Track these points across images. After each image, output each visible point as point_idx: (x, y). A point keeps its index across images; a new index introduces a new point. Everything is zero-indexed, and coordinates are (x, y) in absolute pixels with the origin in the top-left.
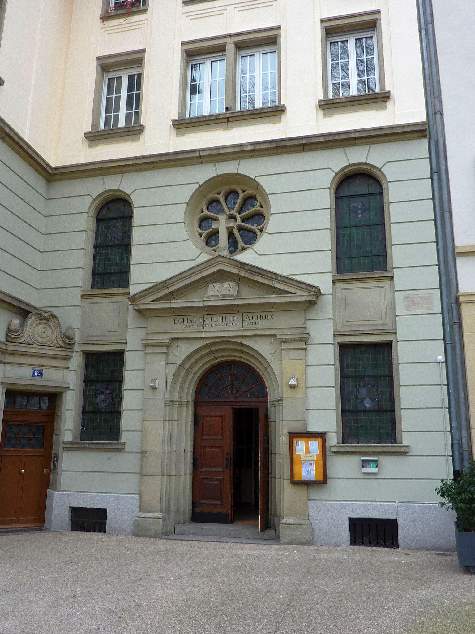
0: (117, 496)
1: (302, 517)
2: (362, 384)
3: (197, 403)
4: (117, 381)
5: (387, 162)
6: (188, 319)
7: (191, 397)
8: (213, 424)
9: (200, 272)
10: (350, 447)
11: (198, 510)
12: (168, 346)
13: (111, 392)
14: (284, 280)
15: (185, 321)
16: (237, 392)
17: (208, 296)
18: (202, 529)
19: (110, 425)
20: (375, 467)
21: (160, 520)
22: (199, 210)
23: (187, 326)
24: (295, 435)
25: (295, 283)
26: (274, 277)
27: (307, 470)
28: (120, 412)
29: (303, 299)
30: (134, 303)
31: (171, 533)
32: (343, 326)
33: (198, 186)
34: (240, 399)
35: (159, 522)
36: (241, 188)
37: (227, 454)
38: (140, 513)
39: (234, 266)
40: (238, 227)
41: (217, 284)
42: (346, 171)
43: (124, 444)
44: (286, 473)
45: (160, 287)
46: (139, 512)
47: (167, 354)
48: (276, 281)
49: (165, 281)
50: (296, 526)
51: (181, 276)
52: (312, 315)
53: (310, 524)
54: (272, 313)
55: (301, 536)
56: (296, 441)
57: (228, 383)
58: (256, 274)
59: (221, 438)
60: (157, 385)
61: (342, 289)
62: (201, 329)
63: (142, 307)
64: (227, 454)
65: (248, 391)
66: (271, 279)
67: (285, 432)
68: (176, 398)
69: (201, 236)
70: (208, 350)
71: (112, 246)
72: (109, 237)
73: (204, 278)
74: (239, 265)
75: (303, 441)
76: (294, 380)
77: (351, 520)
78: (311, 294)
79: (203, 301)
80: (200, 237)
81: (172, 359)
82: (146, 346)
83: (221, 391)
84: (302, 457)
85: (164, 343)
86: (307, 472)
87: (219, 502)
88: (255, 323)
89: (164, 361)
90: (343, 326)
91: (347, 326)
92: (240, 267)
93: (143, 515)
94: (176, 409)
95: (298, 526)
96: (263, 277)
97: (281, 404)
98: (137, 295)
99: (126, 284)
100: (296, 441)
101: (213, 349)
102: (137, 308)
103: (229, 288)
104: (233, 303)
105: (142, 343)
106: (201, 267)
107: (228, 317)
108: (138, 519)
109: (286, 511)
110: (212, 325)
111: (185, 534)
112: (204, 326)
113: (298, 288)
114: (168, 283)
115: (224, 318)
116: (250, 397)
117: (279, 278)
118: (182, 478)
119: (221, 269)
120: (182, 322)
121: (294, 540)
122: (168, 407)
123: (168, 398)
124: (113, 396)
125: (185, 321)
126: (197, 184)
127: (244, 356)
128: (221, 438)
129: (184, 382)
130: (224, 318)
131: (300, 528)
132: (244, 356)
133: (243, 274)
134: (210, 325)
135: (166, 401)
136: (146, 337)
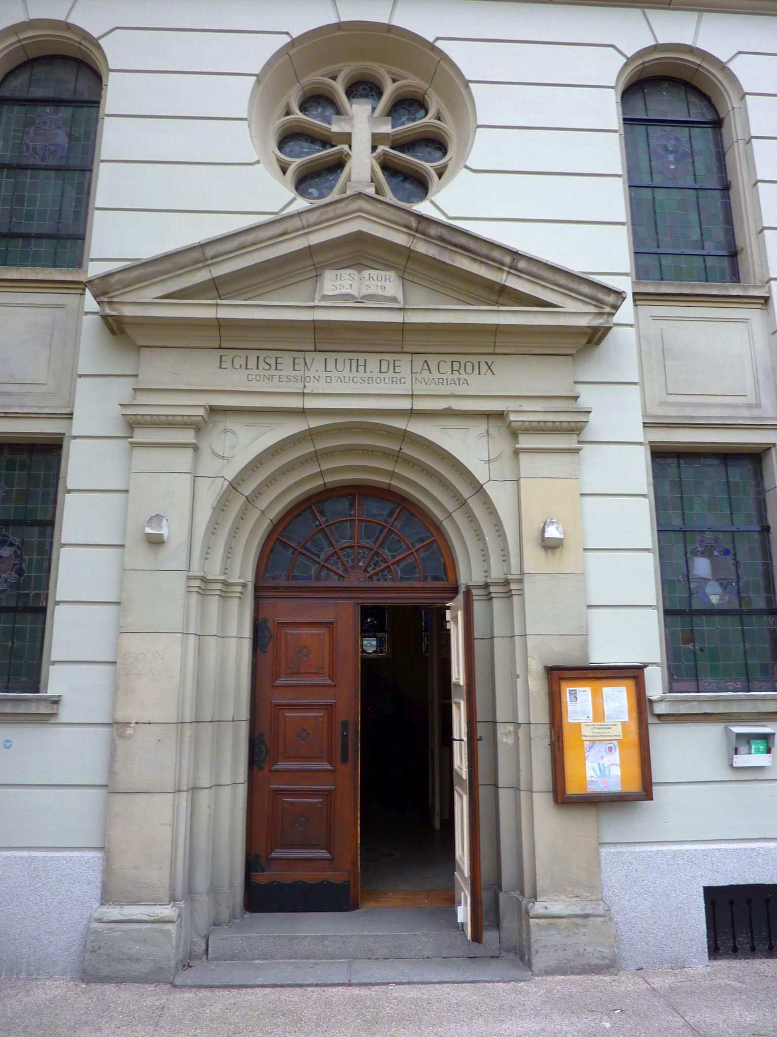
0: (30, 857)
1: (585, 894)
2: (698, 547)
3: (260, 590)
4: (35, 523)
5: (740, 53)
6: (261, 360)
7: (249, 576)
8: (305, 647)
9: (303, 232)
10: (699, 701)
11: (262, 878)
12: (198, 427)
13: (15, 552)
14: (534, 269)
15: (252, 363)
16: (368, 565)
17: (325, 297)
18: (291, 939)
19: (10, 644)
20: (762, 752)
21: (170, 927)
22: (281, 108)
23: (258, 378)
24: (568, 674)
25: (562, 280)
26: (507, 260)
27: (599, 764)
28: (44, 610)
29: (584, 322)
30: (106, 299)
31: (198, 957)
32: (662, 404)
33: (286, 39)
34: (375, 583)
35: (167, 933)
36: (389, 73)
37: (345, 725)
38: (104, 909)
39: (397, 227)
40: (382, 158)
41: (348, 271)
42: (647, 59)
43: (56, 701)
44: (541, 775)
45: (186, 259)
46: (102, 904)
47: (195, 448)
49: (202, 246)
50: (574, 920)
51: (249, 238)
52: (590, 370)
53: (607, 916)
54: (490, 359)
55: (590, 949)
56: (567, 689)
57: (345, 543)
58: (460, 251)
59: (329, 682)
60: (164, 531)
61: (656, 318)
62: (297, 387)
63: (128, 311)
64: (345, 725)
65: (397, 563)
66: (499, 266)
67: (536, 666)
68: (215, 573)
69: (284, 171)
70: (307, 449)
71: (35, 168)
72: (28, 145)
73: (310, 251)
74: (414, 224)
75: (588, 690)
76: (557, 528)
77: (709, 892)
78: (602, 310)
80: (282, 174)
81: (209, 466)
82: (133, 424)
83: (325, 561)
84: (586, 731)
85: (189, 416)
86: (600, 770)
87: (324, 854)
88: (445, 381)
89: (187, 467)
90: (662, 404)
91: (667, 404)
92: (417, 231)
93: (114, 912)
94: (214, 603)
95: (580, 921)
96: (475, 260)
97: (520, 592)
98: (117, 277)
99: (78, 263)
100: (567, 689)
101: (321, 445)
102: (114, 313)
103: (383, 283)
104: (396, 318)
105: (123, 415)
106: (307, 220)
107: (373, 362)
108: (95, 925)
109: (543, 882)
110: (329, 379)
111: (239, 959)
112: (305, 379)
113: (570, 293)
114: (210, 252)
115: (361, 362)
116: (402, 579)
117: (522, 265)
118: (226, 793)
119: (360, 231)
120: (243, 367)
121: (569, 961)
122: (194, 598)
123: (196, 570)
124: (21, 564)
125: (252, 363)
126: (285, 36)
127: (401, 470)
128: (329, 682)
129: (235, 532)
130: (361, 362)
131: (585, 926)
132: (401, 470)
133: (422, 247)
134: (322, 380)
135: (189, 578)
136: (134, 398)
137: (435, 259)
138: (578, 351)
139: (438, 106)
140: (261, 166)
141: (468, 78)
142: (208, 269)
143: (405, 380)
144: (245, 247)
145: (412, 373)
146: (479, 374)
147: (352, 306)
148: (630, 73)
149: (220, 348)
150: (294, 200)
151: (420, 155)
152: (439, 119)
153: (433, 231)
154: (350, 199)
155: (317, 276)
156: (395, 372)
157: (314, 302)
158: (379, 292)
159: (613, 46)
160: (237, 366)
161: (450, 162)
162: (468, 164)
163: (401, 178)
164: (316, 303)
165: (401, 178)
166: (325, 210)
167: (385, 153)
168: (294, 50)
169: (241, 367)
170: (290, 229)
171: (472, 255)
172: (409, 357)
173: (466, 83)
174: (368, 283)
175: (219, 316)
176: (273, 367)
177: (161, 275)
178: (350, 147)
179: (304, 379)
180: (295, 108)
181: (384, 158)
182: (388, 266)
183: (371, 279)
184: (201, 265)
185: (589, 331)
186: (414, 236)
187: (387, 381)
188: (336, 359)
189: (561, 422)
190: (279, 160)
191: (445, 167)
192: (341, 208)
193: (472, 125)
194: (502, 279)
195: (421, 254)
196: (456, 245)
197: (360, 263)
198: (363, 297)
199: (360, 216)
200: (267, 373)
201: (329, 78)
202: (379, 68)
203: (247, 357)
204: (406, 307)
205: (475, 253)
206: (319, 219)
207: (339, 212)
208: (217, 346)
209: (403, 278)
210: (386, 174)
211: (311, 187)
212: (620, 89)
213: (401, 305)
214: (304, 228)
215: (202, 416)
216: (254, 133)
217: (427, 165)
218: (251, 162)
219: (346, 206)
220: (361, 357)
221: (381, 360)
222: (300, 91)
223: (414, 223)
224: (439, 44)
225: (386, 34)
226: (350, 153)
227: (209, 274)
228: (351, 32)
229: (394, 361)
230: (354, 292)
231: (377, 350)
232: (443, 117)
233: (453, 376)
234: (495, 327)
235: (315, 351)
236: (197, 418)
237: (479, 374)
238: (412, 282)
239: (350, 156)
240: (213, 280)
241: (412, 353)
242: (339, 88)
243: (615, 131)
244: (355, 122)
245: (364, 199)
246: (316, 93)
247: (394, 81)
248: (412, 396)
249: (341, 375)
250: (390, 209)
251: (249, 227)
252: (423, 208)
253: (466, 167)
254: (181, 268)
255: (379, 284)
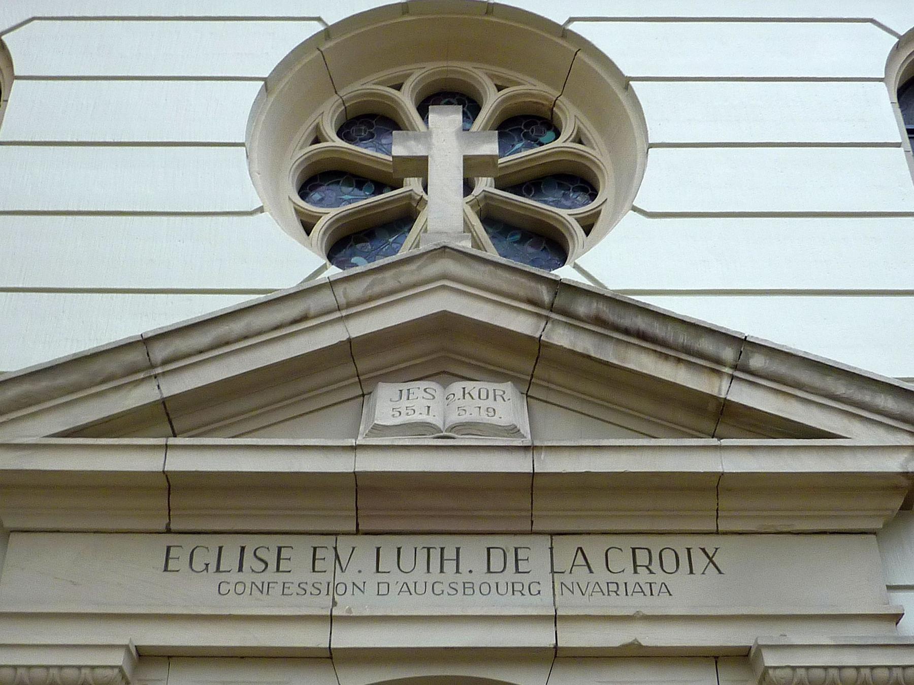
6: (248, 554)
9: (337, 315)
15: (230, 560)
22: (306, 130)
25: (840, 388)
26: (728, 354)
33: (318, 27)
36: (491, 77)
48: (738, 374)
49: (146, 342)
51: (237, 327)
54: (710, 543)
62: (319, 606)
66: (713, 365)
69: (308, 229)
74: (546, 297)
79: (351, 447)
88: (622, 588)
92: (551, 308)
96: (667, 357)
103: (490, 403)
104: (520, 464)
106: (345, 294)
112: (335, 588)
114: (160, 352)
115: (450, 554)
117: (757, 362)
120: (213, 567)
125: (230, 560)
130: (450, 554)
134: (371, 588)
137: (589, 357)
138: (886, 525)
139: (578, 122)
140: (266, 215)
141: (627, 73)
142: (154, 383)
143: (538, 588)
144: (227, 343)
145: (553, 572)
146: (691, 572)
147: (430, 444)
148: (897, 76)
149: (169, 531)
150: (323, 268)
151: (551, 199)
152: (580, 142)
153: (583, 308)
154: (425, 257)
155: (363, 395)
156: (517, 571)
157: (356, 439)
158: (484, 418)
159: (872, 21)
160: (198, 565)
161: (603, 207)
162: (636, 203)
163: (518, 237)
164: (361, 441)
165: (518, 237)
166: (379, 276)
167: (487, 196)
168: (330, 44)
169: (207, 569)
170: (312, 312)
171: (659, 349)
172: (546, 541)
173: (626, 83)
174: (461, 403)
175: (168, 468)
176: (272, 565)
177: (61, 396)
178: (425, 189)
179: (332, 588)
180: (330, 131)
181: (487, 204)
182: (499, 375)
183: (467, 396)
184: (141, 376)
185: (905, 482)
186: (548, 319)
187: (502, 589)
188: (399, 549)
189: (872, 668)
190: (299, 212)
191: (596, 215)
192: (408, 274)
193: (640, 145)
194: (720, 390)
195: (561, 348)
196: (626, 332)
197: (444, 372)
198: (452, 428)
199: (443, 287)
200: (259, 579)
201: (390, 87)
202: (474, 70)
203: (220, 548)
204: (537, 443)
205: (663, 343)
206: (369, 292)
207: (405, 279)
208: (162, 527)
209: (527, 396)
210: (490, 230)
211: (352, 256)
212: (894, 85)
213: (527, 442)
214: (339, 309)
215: (120, 668)
216: (256, 167)
217: (564, 212)
218: (249, 210)
219: (419, 268)
220: (450, 544)
221: (489, 549)
222: (338, 107)
223: (545, 295)
224: (574, 27)
225: (486, 18)
226: (425, 196)
227: (157, 391)
228: (422, 17)
229: (516, 549)
230: (435, 419)
231: (480, 528)
232: (588, 139)
233: (636, 579)
234: (716, 479)
235: (358, 532)
236: (109, 672)
237: (691, 572)
238: (546, 402)
239: (426, 202)
240: (164, 402)
241: (552, 534)
242: (406, 101)
243: (898, 145)
244: (435, 140)
245: (452, 258)
246: (368, 110)
247: (499, 88)
248: (555, 618)
249: (410, 579)
250: (500, 272)
251: (238, 308)
252: (565, 273)
253: (635, 209)
254: (103, 382)
255: (484, 404)
